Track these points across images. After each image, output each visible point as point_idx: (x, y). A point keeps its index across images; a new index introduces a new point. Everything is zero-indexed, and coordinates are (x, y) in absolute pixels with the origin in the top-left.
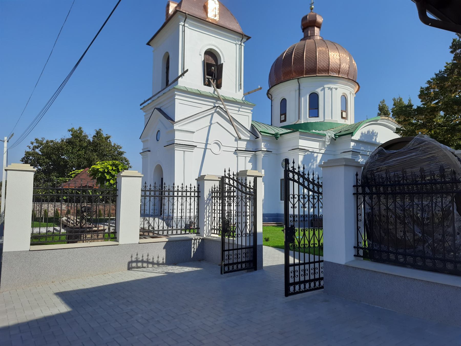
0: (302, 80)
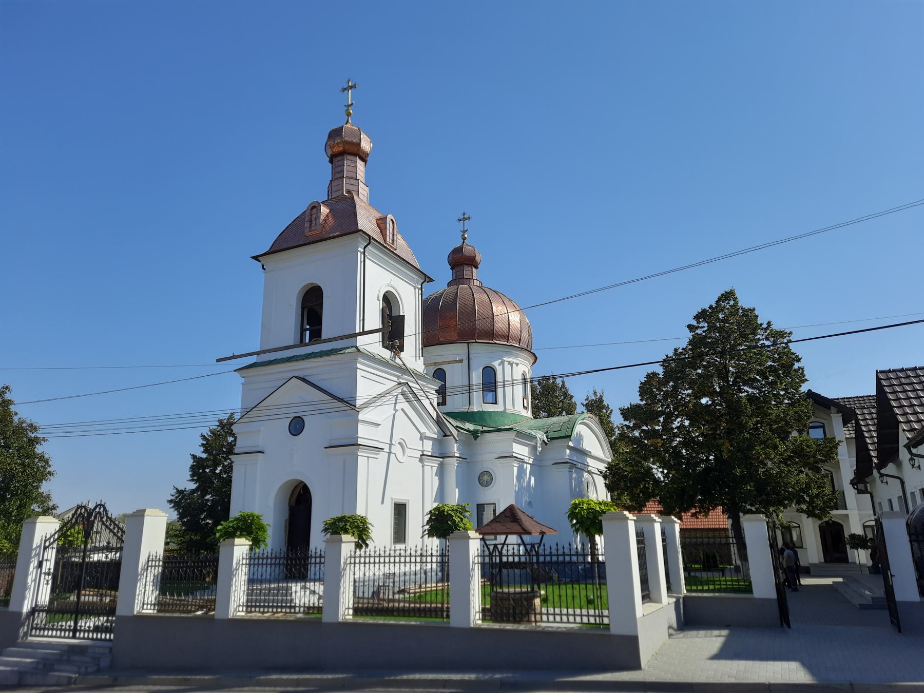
0: (472, 346)
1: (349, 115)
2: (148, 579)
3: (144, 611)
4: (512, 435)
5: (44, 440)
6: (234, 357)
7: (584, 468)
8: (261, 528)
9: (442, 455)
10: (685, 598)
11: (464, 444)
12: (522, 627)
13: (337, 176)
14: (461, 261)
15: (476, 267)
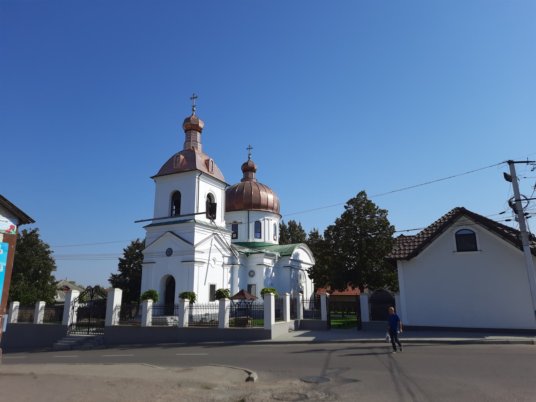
0: (251, 212)
1: (194, 110)
4: (263, 255)
5: (52, 252)
6: (142, 221)
7: (299, 268)
8: (156, 295)
9: (232, 263)
10: (301, 321)
13: (188, 140)
15: (255, 172)
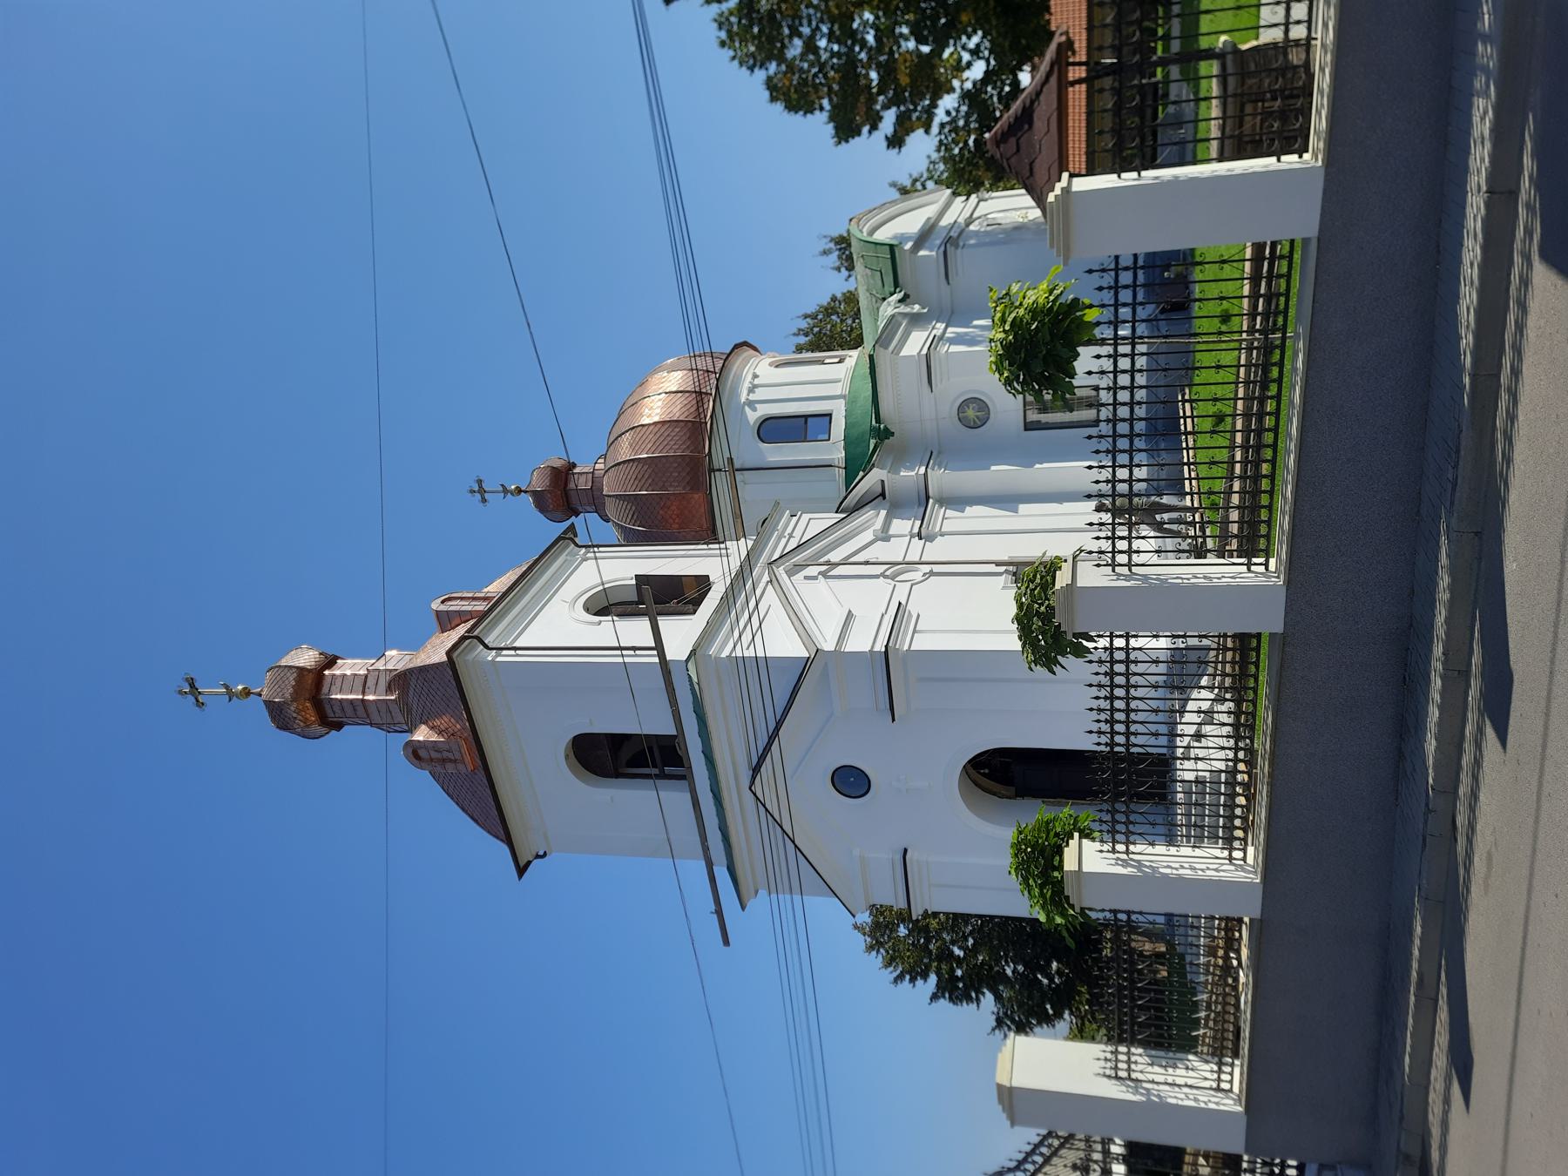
2: (1161, 1079)
3: (1236, 1089)
11: (902, 457)
12: (1323, 81)
14: (562, 496)
15: (574, 466)
